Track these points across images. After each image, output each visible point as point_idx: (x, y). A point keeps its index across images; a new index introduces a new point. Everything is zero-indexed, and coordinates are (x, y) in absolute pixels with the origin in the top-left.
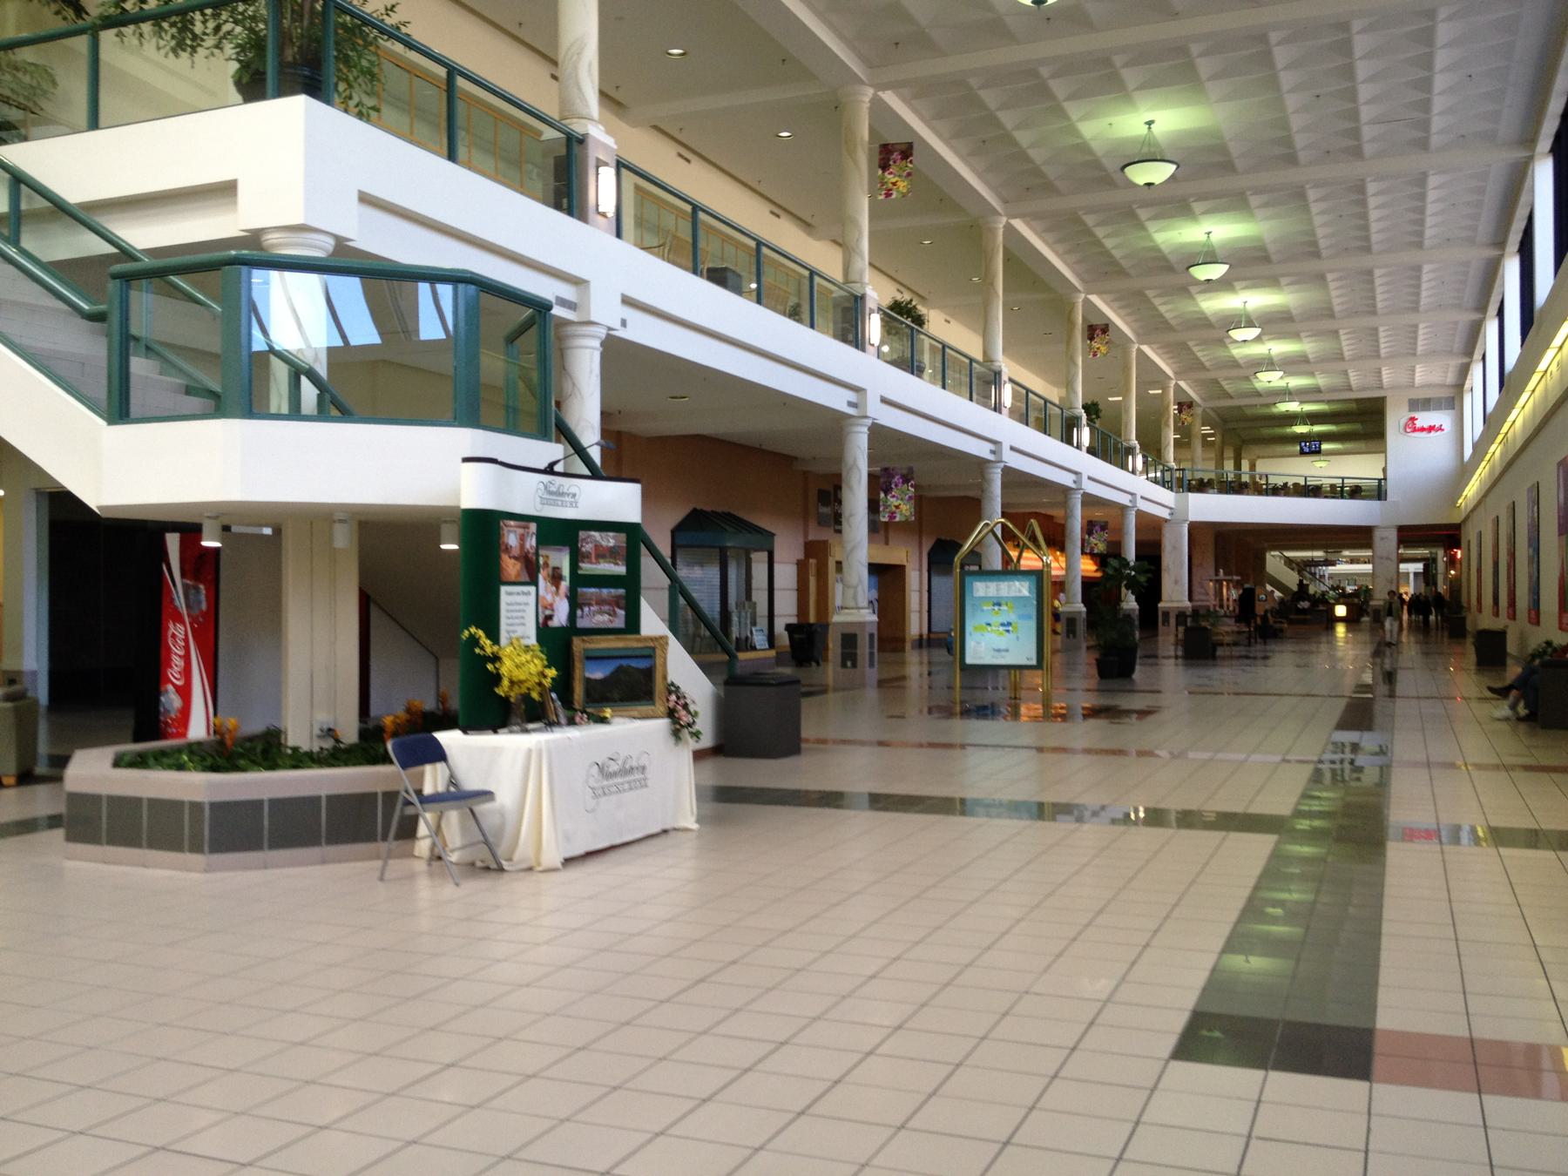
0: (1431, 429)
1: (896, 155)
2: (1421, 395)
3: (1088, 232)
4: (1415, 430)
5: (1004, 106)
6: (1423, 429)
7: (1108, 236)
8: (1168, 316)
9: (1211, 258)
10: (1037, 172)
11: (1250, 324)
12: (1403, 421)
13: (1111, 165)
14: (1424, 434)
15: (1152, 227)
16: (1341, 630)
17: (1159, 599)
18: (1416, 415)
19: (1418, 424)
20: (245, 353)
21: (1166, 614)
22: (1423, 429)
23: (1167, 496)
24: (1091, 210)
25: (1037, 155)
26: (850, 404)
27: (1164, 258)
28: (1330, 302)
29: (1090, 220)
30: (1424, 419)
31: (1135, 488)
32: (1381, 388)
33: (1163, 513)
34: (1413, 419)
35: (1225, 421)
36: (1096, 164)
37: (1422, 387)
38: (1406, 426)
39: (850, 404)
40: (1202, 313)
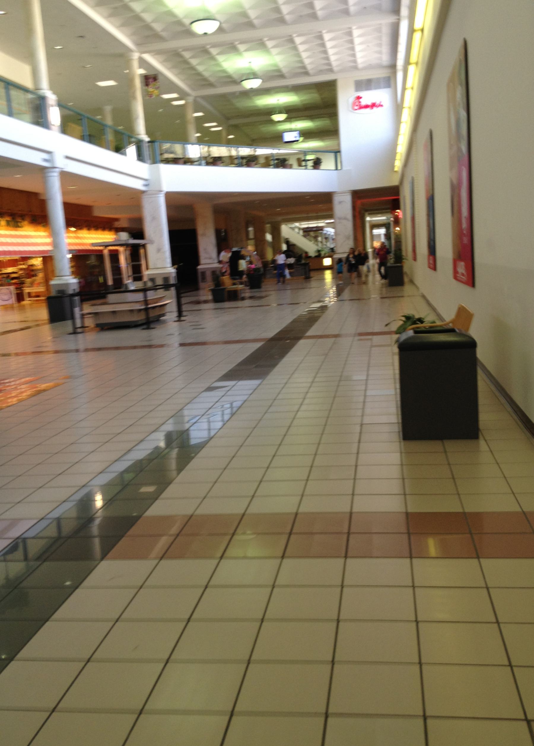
0: (373, 105)
1: (151, 80)
2: (364, 76)
3: (186, 62)
4: (361, 107)
5: (193, 57)
6: (367, 107)
7: (198, 64)
8: (206, 74)
9: (254, 75)
10: (148, 27)
11: (280, 112)
12: (352, 99)
13: (187, 22)
14: (368, 110)
15: (221, 59)
16: (328, 275)
17: (198, 263)
18: (360, 94)
19: (363, 102)
20: (280, 218)
21: (203, 273)
22: (367, 107)
23: (144, 169)
24: (186, 49)
25: (148, 17)
26: (46, 160)
27: (229, 77)
28: (301, 62)
29: (187, 55)
30: (368, 97)
31: (121, 169)
32: (331, 70)
33: (138, 185)
34: (359, 98)
35: (228, 119)
36: (179, 23)
37: (365, 68)
38: (354, 104)
39: (46, 160)
40: (224, 71)
